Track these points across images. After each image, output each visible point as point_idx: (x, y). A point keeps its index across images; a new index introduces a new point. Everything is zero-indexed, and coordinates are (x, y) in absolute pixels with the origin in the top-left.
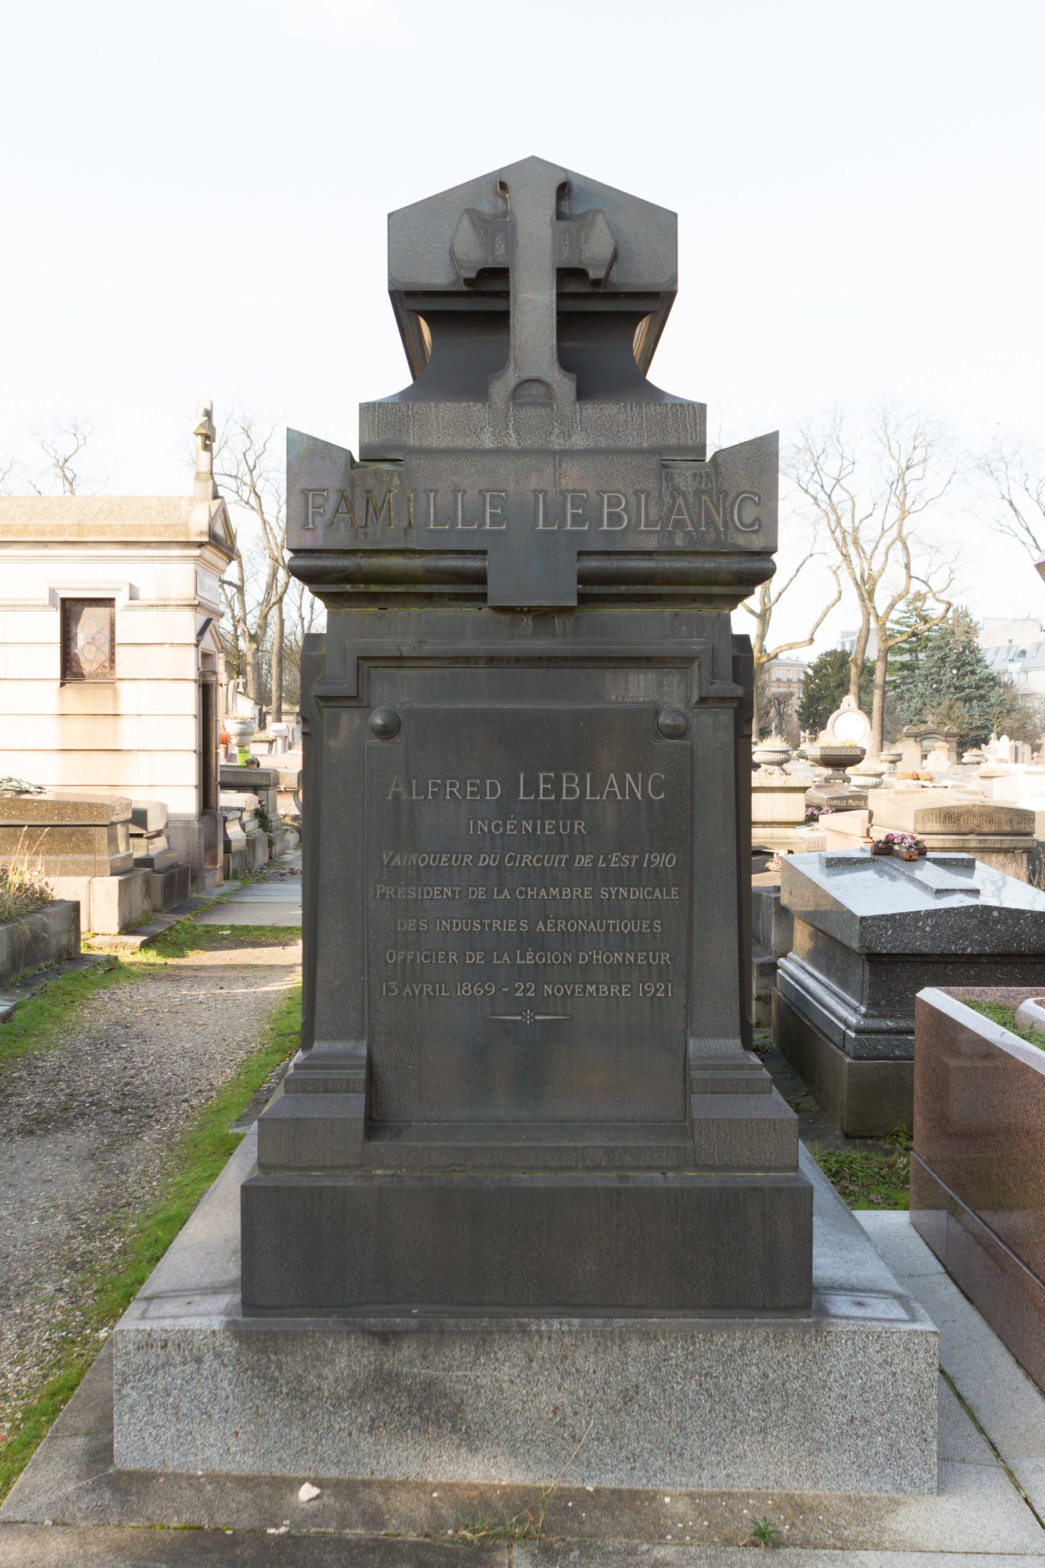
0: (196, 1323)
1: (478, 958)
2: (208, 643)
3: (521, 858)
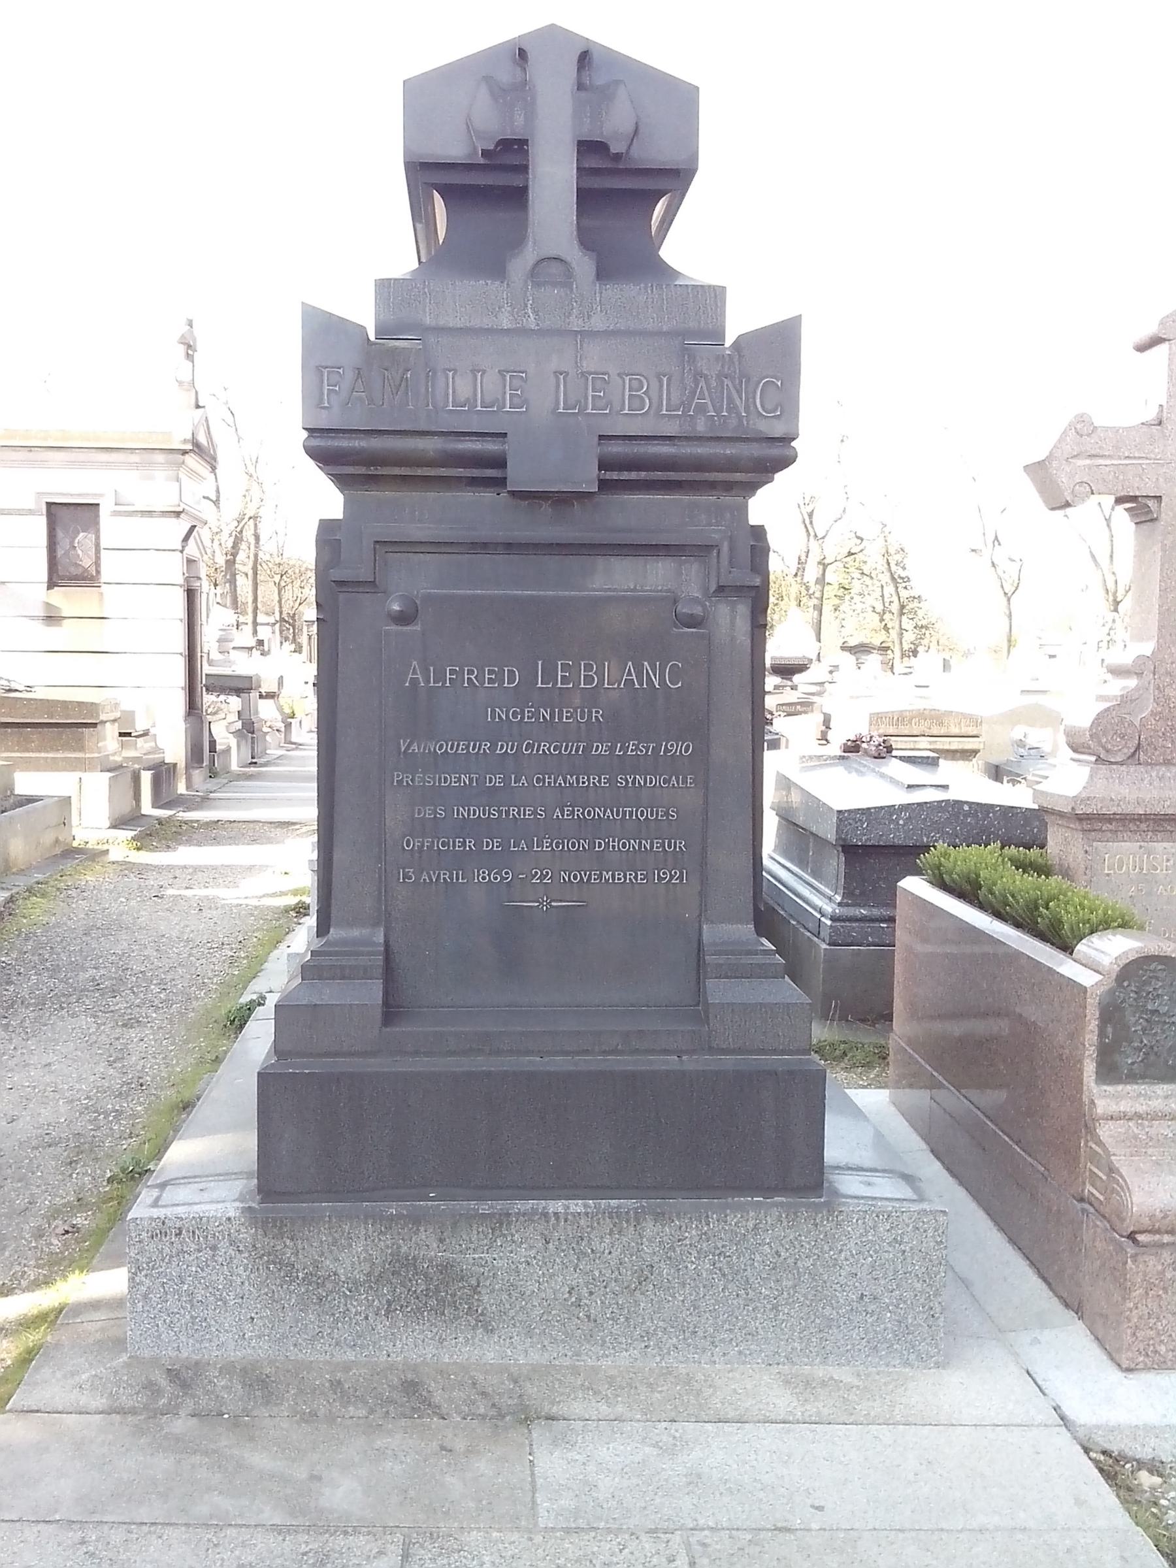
0: (210, 1210)
2: (192, 549)
3: (539, 746)
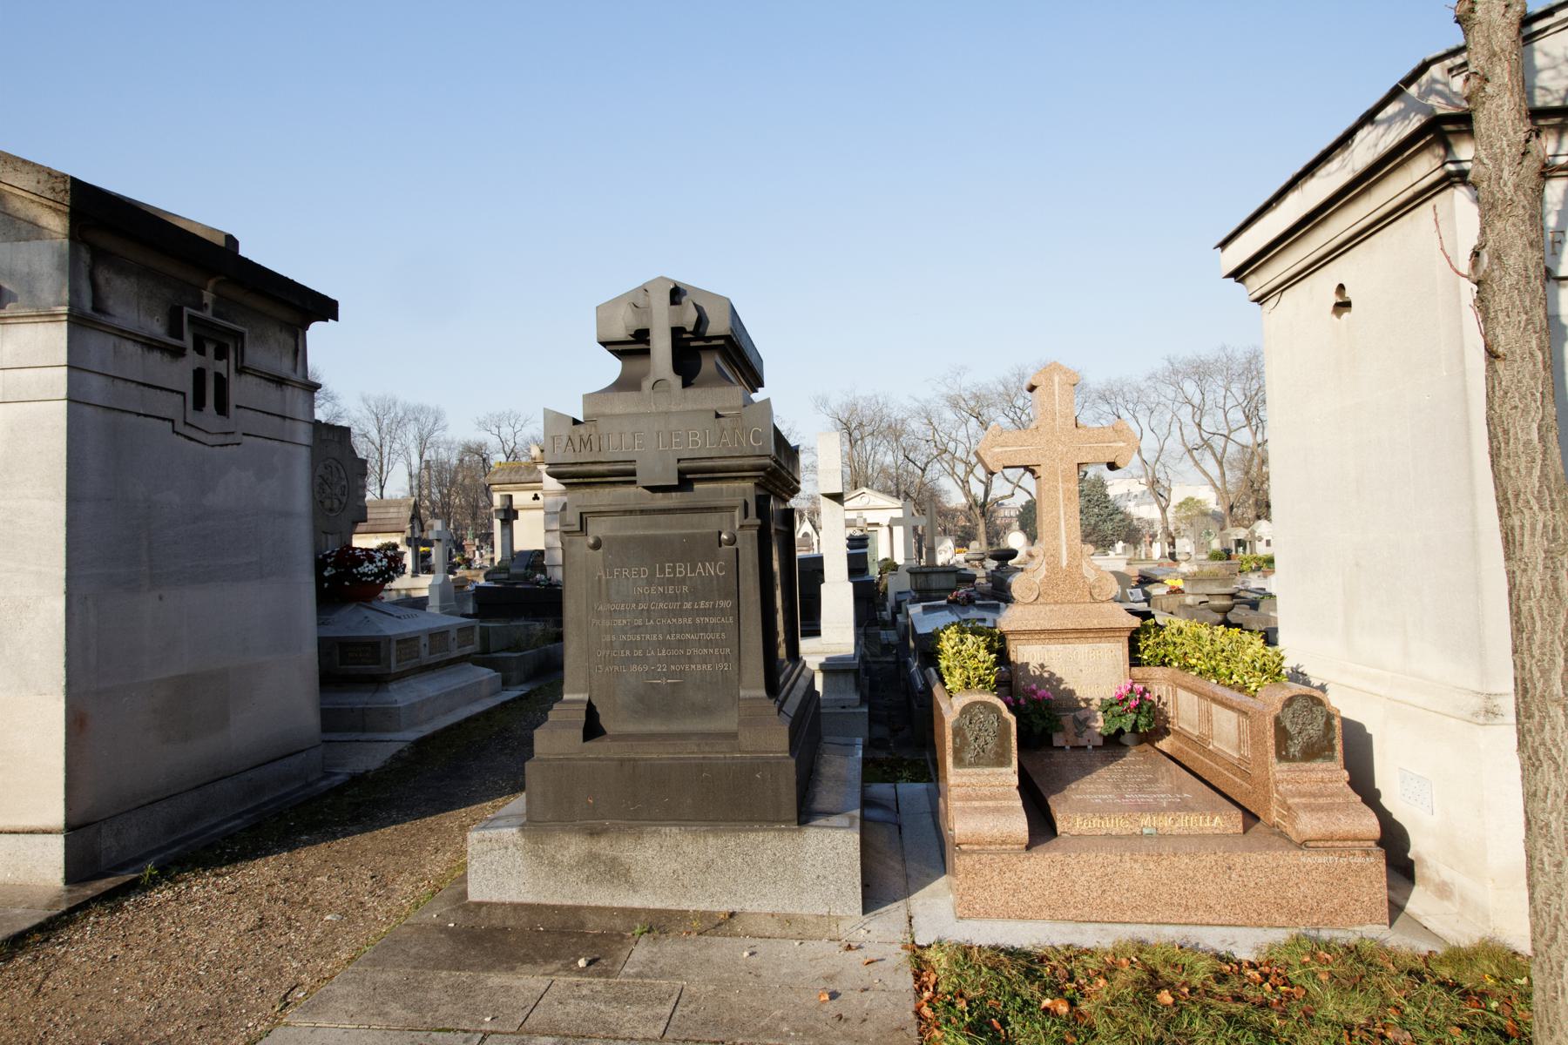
1: (640, 653)
